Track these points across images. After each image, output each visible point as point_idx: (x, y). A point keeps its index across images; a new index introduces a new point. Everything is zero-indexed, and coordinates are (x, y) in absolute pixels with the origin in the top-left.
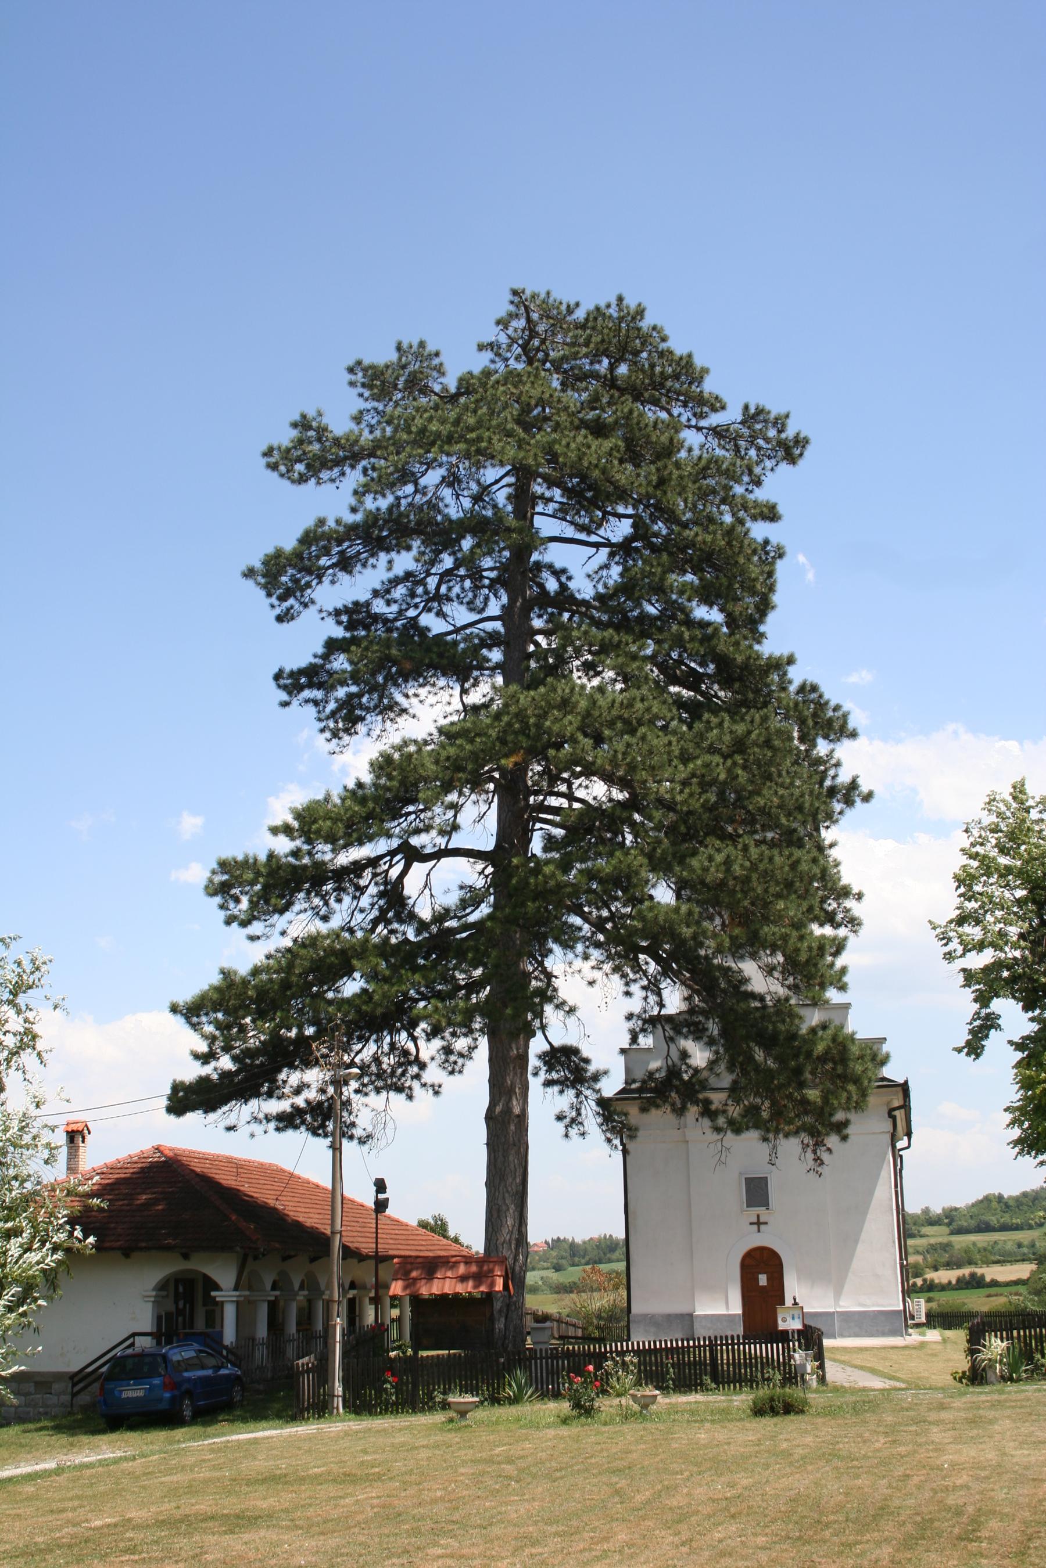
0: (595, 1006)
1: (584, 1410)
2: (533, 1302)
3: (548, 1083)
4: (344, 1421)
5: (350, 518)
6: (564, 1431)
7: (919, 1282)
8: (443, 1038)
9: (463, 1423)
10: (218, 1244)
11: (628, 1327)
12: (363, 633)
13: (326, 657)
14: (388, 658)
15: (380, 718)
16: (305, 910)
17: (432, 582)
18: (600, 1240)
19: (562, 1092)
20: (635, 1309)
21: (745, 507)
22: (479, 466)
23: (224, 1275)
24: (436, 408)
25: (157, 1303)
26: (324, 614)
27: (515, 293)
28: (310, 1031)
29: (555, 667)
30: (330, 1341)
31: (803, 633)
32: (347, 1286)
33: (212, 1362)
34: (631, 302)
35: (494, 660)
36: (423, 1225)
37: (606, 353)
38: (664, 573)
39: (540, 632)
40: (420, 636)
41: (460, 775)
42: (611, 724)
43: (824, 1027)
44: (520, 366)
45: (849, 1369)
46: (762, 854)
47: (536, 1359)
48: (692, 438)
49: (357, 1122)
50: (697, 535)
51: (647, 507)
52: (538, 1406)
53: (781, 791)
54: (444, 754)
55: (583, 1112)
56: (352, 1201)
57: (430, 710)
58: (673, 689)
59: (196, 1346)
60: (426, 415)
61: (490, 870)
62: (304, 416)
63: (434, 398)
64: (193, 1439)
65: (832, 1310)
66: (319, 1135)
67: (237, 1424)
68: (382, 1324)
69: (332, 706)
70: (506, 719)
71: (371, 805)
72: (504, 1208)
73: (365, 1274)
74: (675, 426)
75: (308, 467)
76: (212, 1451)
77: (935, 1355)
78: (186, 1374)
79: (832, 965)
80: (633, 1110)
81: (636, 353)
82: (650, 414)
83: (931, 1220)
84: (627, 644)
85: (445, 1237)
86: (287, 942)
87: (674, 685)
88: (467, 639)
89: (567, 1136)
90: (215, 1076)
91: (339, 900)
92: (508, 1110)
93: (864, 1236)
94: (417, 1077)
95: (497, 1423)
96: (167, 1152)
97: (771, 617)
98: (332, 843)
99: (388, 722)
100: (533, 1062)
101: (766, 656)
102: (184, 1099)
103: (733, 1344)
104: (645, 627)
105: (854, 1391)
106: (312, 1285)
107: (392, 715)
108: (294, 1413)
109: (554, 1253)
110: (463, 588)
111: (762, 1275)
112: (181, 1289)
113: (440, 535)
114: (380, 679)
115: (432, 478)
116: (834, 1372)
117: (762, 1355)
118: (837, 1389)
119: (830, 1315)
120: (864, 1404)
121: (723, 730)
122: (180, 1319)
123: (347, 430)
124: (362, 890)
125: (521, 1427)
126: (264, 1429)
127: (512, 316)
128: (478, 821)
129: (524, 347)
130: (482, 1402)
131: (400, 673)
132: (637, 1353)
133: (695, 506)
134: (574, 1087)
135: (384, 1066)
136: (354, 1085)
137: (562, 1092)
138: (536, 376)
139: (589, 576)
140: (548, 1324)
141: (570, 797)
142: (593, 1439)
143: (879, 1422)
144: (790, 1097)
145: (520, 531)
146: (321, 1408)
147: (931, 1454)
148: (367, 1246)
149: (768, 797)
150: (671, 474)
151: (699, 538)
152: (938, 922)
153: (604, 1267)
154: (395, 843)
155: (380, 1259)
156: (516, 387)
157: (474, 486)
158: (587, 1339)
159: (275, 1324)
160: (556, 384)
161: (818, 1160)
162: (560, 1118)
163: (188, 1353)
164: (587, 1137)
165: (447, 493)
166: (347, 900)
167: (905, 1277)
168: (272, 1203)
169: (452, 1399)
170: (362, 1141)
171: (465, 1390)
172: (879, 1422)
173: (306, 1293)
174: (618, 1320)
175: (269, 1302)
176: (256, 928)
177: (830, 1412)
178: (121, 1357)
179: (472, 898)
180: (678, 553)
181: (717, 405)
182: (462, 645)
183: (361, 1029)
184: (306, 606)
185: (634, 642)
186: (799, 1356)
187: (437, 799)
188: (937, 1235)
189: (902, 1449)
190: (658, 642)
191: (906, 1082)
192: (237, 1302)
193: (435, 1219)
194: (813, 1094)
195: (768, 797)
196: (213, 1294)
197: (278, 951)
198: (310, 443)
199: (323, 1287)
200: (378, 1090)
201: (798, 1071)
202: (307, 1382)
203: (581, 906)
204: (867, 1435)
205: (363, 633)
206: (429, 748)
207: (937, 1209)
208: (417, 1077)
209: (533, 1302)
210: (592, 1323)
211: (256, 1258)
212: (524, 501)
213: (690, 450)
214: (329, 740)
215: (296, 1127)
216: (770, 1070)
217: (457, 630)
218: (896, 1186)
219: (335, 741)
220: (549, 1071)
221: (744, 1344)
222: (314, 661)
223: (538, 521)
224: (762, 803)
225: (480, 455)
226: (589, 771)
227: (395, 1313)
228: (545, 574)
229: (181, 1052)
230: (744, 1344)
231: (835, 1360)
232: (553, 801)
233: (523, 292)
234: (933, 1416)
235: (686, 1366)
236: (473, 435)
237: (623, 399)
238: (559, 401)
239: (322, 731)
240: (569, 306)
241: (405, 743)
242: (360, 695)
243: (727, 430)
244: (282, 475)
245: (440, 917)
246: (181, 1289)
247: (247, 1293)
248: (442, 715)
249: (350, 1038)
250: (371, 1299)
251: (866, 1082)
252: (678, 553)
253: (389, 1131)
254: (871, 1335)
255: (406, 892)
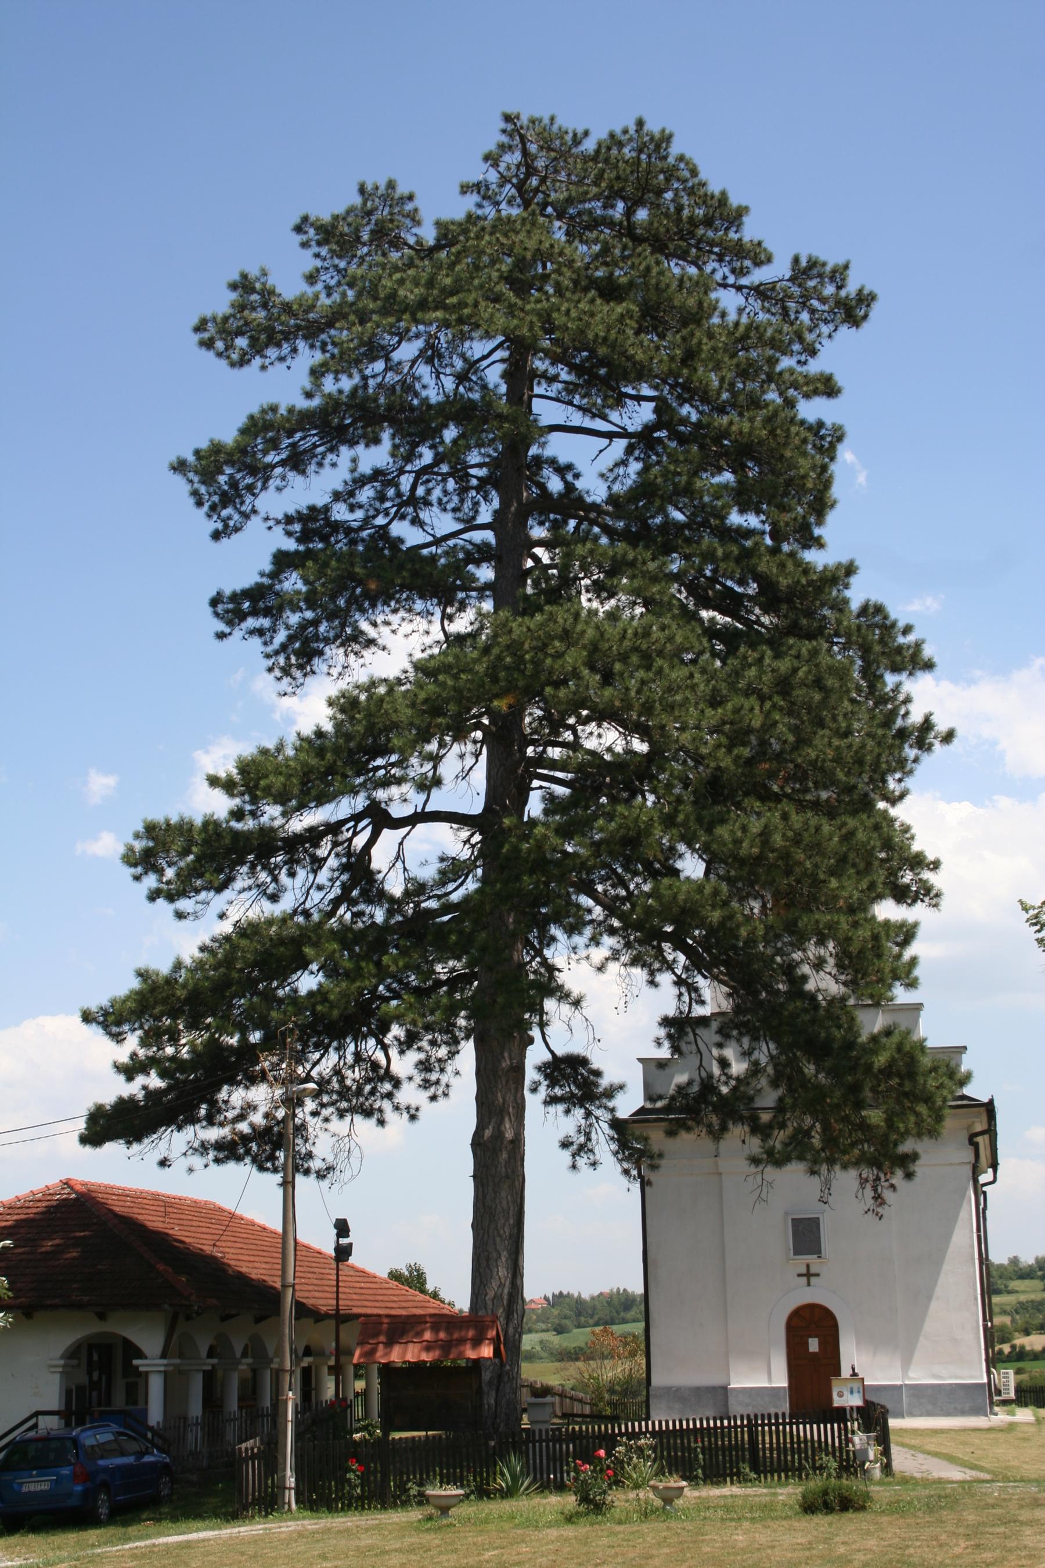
0: (611, 1007)
1: (593, 1506)
2: (531, 1372)
3: (551, 1101)
4: (298, 1519)
5: (303, 404)
6: (569, 1531)
7: (1006, 1348)
8: (419, 1049)
9: (445, 1522)
10: (141, 1299)
11: (647, 1402)
12: (320, 546)
13: (274, 576)
14: (352, 577)
15: (341, 650)
16: (250, 888)
17: (406, 482)
18: (611, 1295)
19: (567, 1112)
20: (656, 1380)
21: (795, 385)
22: (464, 337)
23: (149, 1340)
24: (411, 264)
25: (65, 1374)
26: (271, 523)
27: (508, 118)
28: (255, 1037)
29: (560, 590)
30: (280, 1420)
31: (875, 537)
32: (301, 1352)
33: (134, 1446)
34: (653, 126)
35: (482, 580)
36: (395, 1276)
37: (619, 194)
38: (695, 474)
39: (540, 543)
40: (391, 548)
41: (439, 720)
42: (624, 658)
43: (888, 1032)
44: (515, 212)
45: (920, 1456)
46: (806, 823)
47: (534, 1442)
48: (729, 301)
49: (315, 1151)
50: (731, 423)
51: (672, 387)
52: (537, 1500)
53: (836, 742)
54: (422, 695)
55: (593, 1136)
56: (308, 1248)
57: (401, 643)
58: (704, 614)
59: (115, 1428)
60: (397, 276)
61: (477, 838)
62: (244, 276)
63: (406, 251)
64: (109, 1542)
65: (899, 1383)
66: (267, 1169)
67: (164, 1523)
68: (345, 1399)
69: (281, 637)
70: (495, 651)
71: (329, 756)
72: (495, 1255)
73: (324, 1337)
74: (704, 285)
75: (254, 341)
76: (134, 1557)
77: (1025, 1439)
78: (101, 1462)
79: (899, 956)
80: (657, 1137)
81: (659, 193)
82: (677, 271)
83: (1019, 1272)
84: (644, 563)
85: (423, 1291)
86: (226, 927)
87: (707, 608)
88: (451, 552)
89: (574, 1167)
90: (141, 1095)
91: (292, 874)
92: (499, 1135)
93: (938, 1291)
94: (389, 1096)
95: (486, 1521)
96: (78, 1187)
97: (832, 517)
98: (283, 804)
99: (352, 657)
100: (531, 1074)
101: (820, 568)
102: (109, 1125)
103: (777, 1424)
104: (668, 539)
105: (927, 1483)
106: (257, 1351)
107: (357, 647)
108: (234, 1514)
109: (555, 1312)
110: (445, 492)
111: (812, 1336)
112: (95, 1357)
113: (414, 423)
114: (342, 602)
115: (407, 351)
116: (902, 1460)
117: (815, 1438)
118: (906, 1481)
119: (898, 1388)
120: (941, 1499)
121: (765, 667)
122: (95, 1394)
123: (298, 293)
124: (318, 863)
125: (516, 1526)
126: (198, 1530)
127: (503, 148)
128: (464, 777)
129: (520, 187)
130: (467, 1496)
131: (366, 594)
132: (654, 1434)
133: (732, 385)
134: (582, 1106)
135: (349, 1082)
136: (310, 1105)
137: (567, 1112)
138: (534, 224)
139: (602, 475)
140: (549, 1399)
141: (575, 746)
142: (605, 1541)
143: (959, 1522)
144: (845, 1119)
145: (512, 419)
146: (269, 1504)
147: (1024, 1562)
148: (325, 1303)
149: (821, 747)
150: (700, 343)
151: (734, 428)
152: (1030, 902)
153: (617, 1329)
154: (360, 802)
155: (341, 1318)
156: (506, 235)
157: (459, 364)
158: (597, 1417)
159: (212, 1401)
160: (560, 236)
161: (878, 1197)
162: (565, 1144)
163: (104, 1437)
164: (600, 1168)
165: (423, 370)
166: (301, 873)
167: (989, 1343)
168: (208, 1249)
169: (430, 1491)
170: (321, 1175)
171: (447, 1480)
172: (959, 1522)
173: (250, 1360)
174: (635, 1394)
175: (204, 1371)
176: (185, 904)
177: (897, 1508)
178: (20, 1442)
179: (453, 870)
180: (710, 446)
181: (759, 256)
182: (443, 561)
183: (319, 1034)
184: (246, 516)
185: (653, 560)
186: (859, 1439)
187: (414, 748)
188: (1029, 1291)
189: (987, 1556)
190: (687, 557)
191: (991, 1102)
192: (165, 1372)
193: (409, 1268)
194: (875, 1116)
195: (821, 747)
196: (135, 1362)
197: (214, 940)
198: (254, 309)
199: (271, 1354)
200: (341, 1114)
201: (855, 1088)
202: (251, 1471)
203: (592, 882)
204: (943, 1537)
205: (320, 546)
206: (403, 688)
207: (1028, 1259)
208: (389, 1096)
209: (531, 1372)
210: (602, 1399)
211: (188, 1318)
212: (519, 377)
213: (723, 315)
214: (279, 679)
215: (239, 1159)
216: (818, 1087)
217: (437, 541)
218: (978, 1230)
219: (286, 680)
220: (551, 1086)
221: (791, 1424)
222: (259, 579)
223: (537, 405)
224: (813, 755)
225: (465, 325)
226: (601, 716)
227: (360, 1385)
228: (547, 472)
229: (99, 1069)
230: (791, 1424)
231: (903, 1445)
232: (555, 753)
233: (518, 117)
234: (1025, 1515)
235: (718, 1451)
236: (453, 300)
237: (639, 249)
238: (561, 254)
239: (270, 670)
240: (575, 135)
241: (373, 684)
242: (315, 623)
243: (773, 289)
244: (219, 355)
245: (417, 889)
246: (95, 1357)
247: (177, 1361)
248: (419, 648)
249: (305, 1045)
250: (330, 1368)
251: (939, 1103)
252: (710, 446)
253: (354, 1160)
254: (948, 1414)
255: (374, 865)
